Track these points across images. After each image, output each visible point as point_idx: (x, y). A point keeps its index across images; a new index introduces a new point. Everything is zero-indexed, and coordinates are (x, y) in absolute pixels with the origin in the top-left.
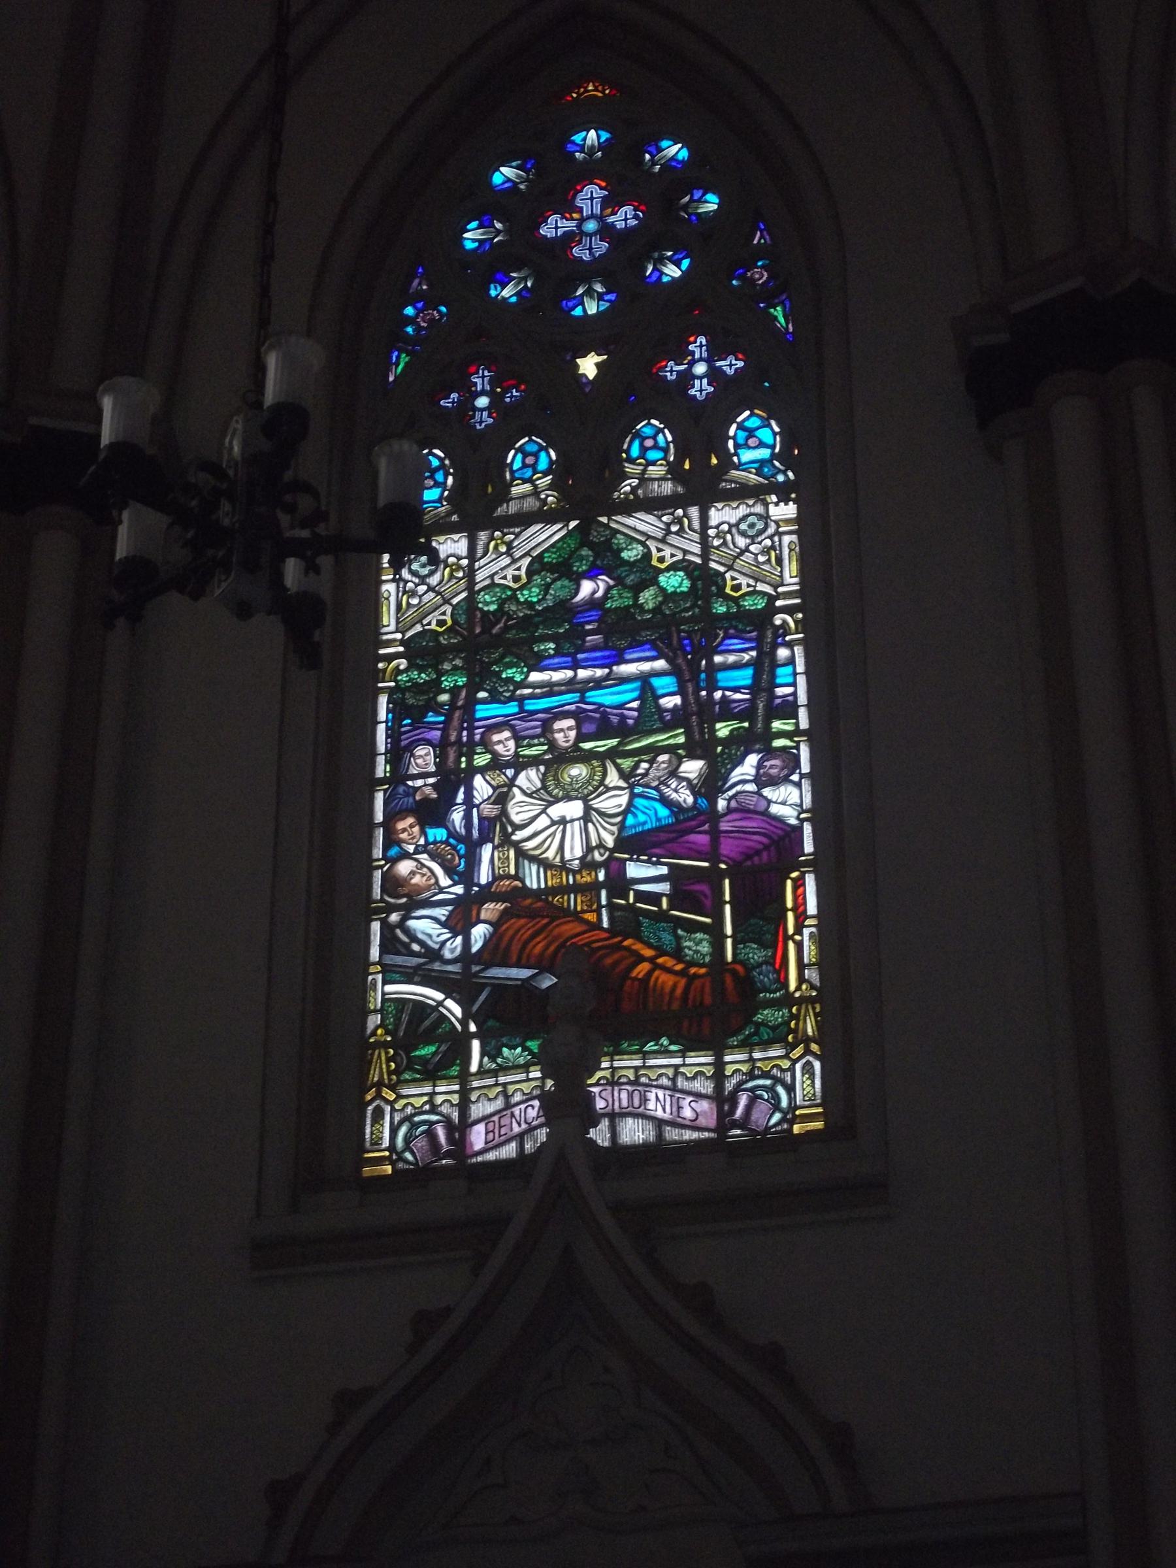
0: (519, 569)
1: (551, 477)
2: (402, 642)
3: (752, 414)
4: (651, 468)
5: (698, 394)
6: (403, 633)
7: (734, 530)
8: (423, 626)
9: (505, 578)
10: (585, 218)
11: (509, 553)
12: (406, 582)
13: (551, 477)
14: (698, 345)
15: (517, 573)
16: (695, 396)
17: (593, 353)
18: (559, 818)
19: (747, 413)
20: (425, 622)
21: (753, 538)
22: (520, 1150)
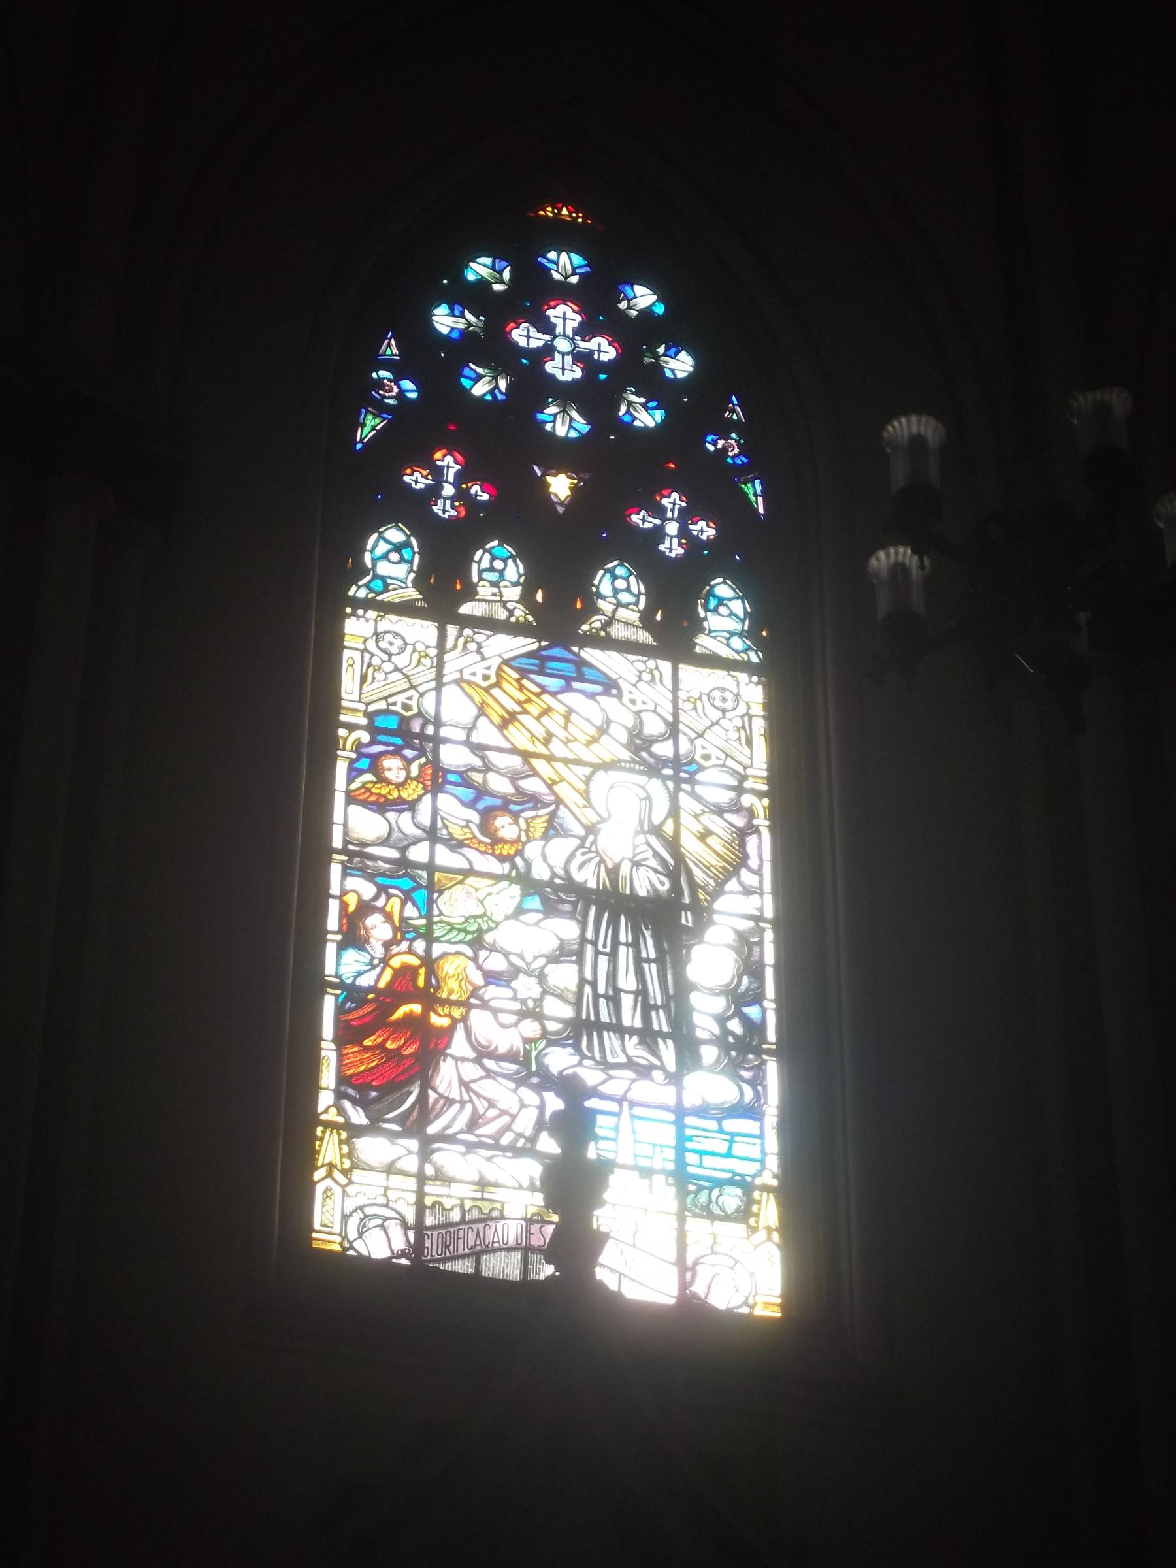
0: (489, 668)
1: (623, 918)
2: (366, 714)
3: (621, 564)
4: (621, 609)
5: (667, 551)
6: (367, 705)
7: (705, 698)
8: (388, 705)
9: (474, 674)
10: (333, 1169)
11: (478, 651)
12: (372, 655)
13: (623, 918)
14: (673, 501)
15: (487, 672)
16: (665, 552)
17: (436, 624)
18: (512, 711)
19: (616, 563)
20: (390, 700)
21: (724, 711)
22: (494, 795)
